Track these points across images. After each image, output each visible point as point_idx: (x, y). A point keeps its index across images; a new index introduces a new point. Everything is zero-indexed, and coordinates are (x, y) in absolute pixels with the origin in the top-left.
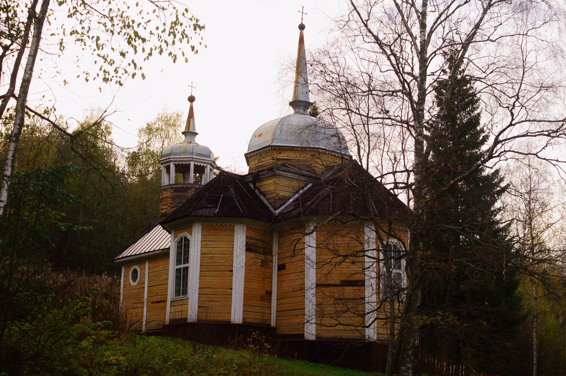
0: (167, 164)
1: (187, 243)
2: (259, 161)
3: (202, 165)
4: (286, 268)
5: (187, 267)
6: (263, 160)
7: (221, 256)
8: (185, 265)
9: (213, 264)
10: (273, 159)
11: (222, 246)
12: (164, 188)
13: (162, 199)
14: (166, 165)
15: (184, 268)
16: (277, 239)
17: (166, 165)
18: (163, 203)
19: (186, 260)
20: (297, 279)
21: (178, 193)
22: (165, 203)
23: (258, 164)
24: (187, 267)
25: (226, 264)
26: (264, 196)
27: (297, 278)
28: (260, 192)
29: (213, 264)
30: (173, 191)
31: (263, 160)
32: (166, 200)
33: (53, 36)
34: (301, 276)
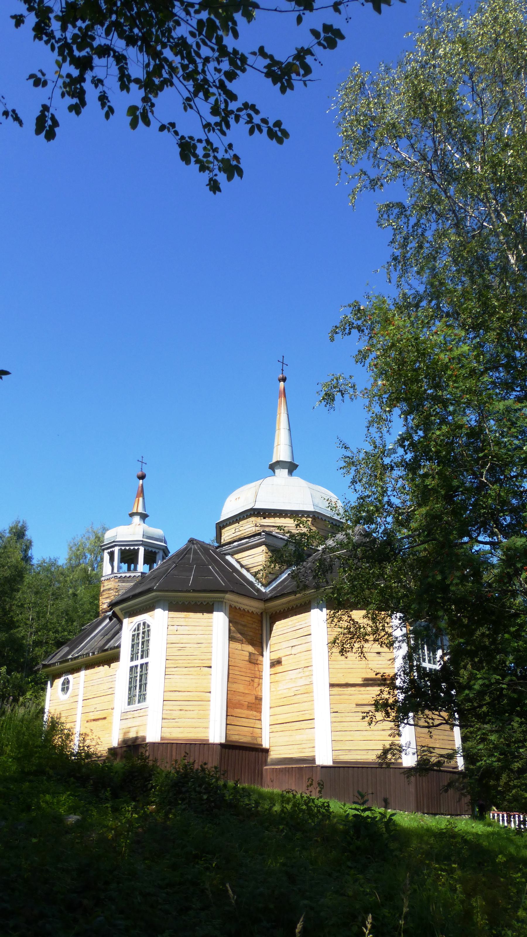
0: (111, 550)
1: (146, 629)
2: (236, 530)
3: (154, 550)
4: (283, 663)
5: (147, 664)
6: (241, 529)
7: (196, 646)
8: (144, 661)
9: (184, 658)
10: (256, 526)
11: (196, 633)
12: (106, 578)
13: (103, 591)
14: (109, 550)
15: (142, 665)
16: (269, 625)
17: (109, 550)
18: (104, 597)
19: (145, 653)
20: (301, 678)
21: (123, 584)
22: (107, 596)
23: (234, 535)
24: (147, 664)
25: (202, 657)
26: (248, 570)
27: (300, 675)
28: (242, 566)
29: (184, 658)
30: (117, 580)
31: (241, 529)
32: (107, 592)
33: (4, 97)
34: (307, 674)
